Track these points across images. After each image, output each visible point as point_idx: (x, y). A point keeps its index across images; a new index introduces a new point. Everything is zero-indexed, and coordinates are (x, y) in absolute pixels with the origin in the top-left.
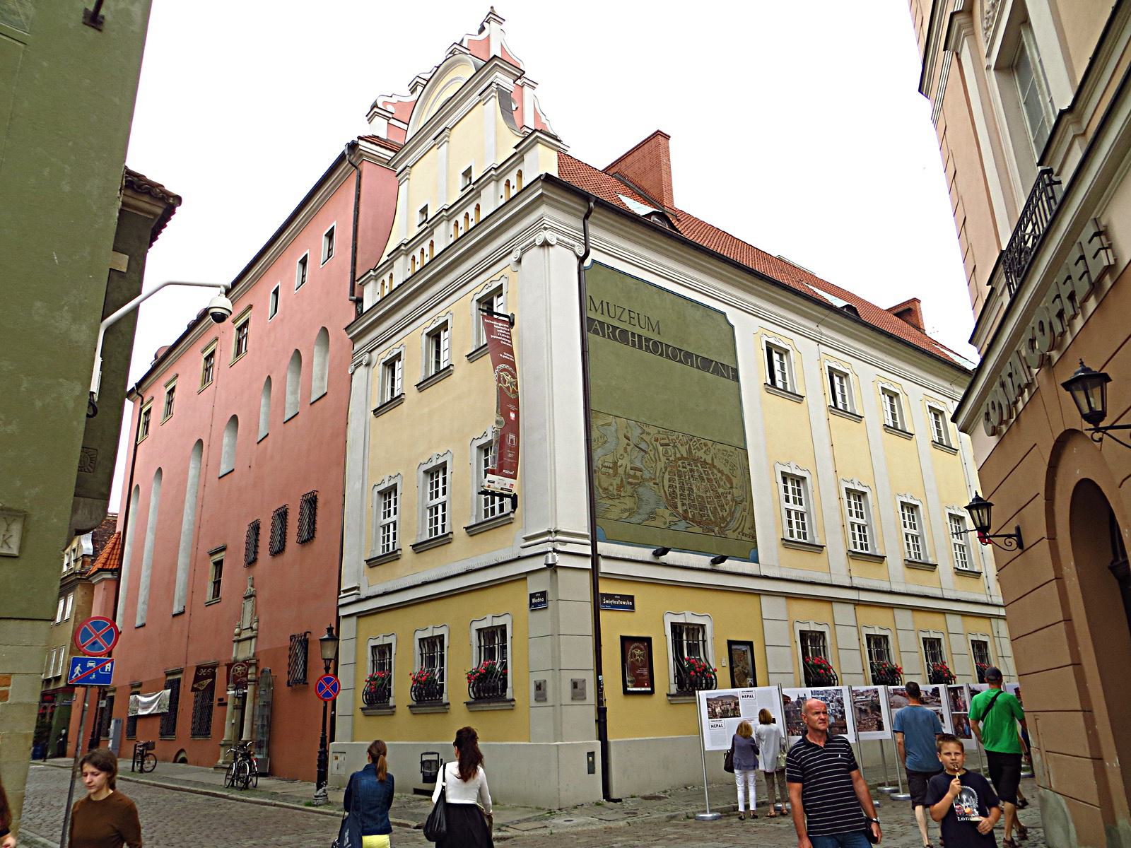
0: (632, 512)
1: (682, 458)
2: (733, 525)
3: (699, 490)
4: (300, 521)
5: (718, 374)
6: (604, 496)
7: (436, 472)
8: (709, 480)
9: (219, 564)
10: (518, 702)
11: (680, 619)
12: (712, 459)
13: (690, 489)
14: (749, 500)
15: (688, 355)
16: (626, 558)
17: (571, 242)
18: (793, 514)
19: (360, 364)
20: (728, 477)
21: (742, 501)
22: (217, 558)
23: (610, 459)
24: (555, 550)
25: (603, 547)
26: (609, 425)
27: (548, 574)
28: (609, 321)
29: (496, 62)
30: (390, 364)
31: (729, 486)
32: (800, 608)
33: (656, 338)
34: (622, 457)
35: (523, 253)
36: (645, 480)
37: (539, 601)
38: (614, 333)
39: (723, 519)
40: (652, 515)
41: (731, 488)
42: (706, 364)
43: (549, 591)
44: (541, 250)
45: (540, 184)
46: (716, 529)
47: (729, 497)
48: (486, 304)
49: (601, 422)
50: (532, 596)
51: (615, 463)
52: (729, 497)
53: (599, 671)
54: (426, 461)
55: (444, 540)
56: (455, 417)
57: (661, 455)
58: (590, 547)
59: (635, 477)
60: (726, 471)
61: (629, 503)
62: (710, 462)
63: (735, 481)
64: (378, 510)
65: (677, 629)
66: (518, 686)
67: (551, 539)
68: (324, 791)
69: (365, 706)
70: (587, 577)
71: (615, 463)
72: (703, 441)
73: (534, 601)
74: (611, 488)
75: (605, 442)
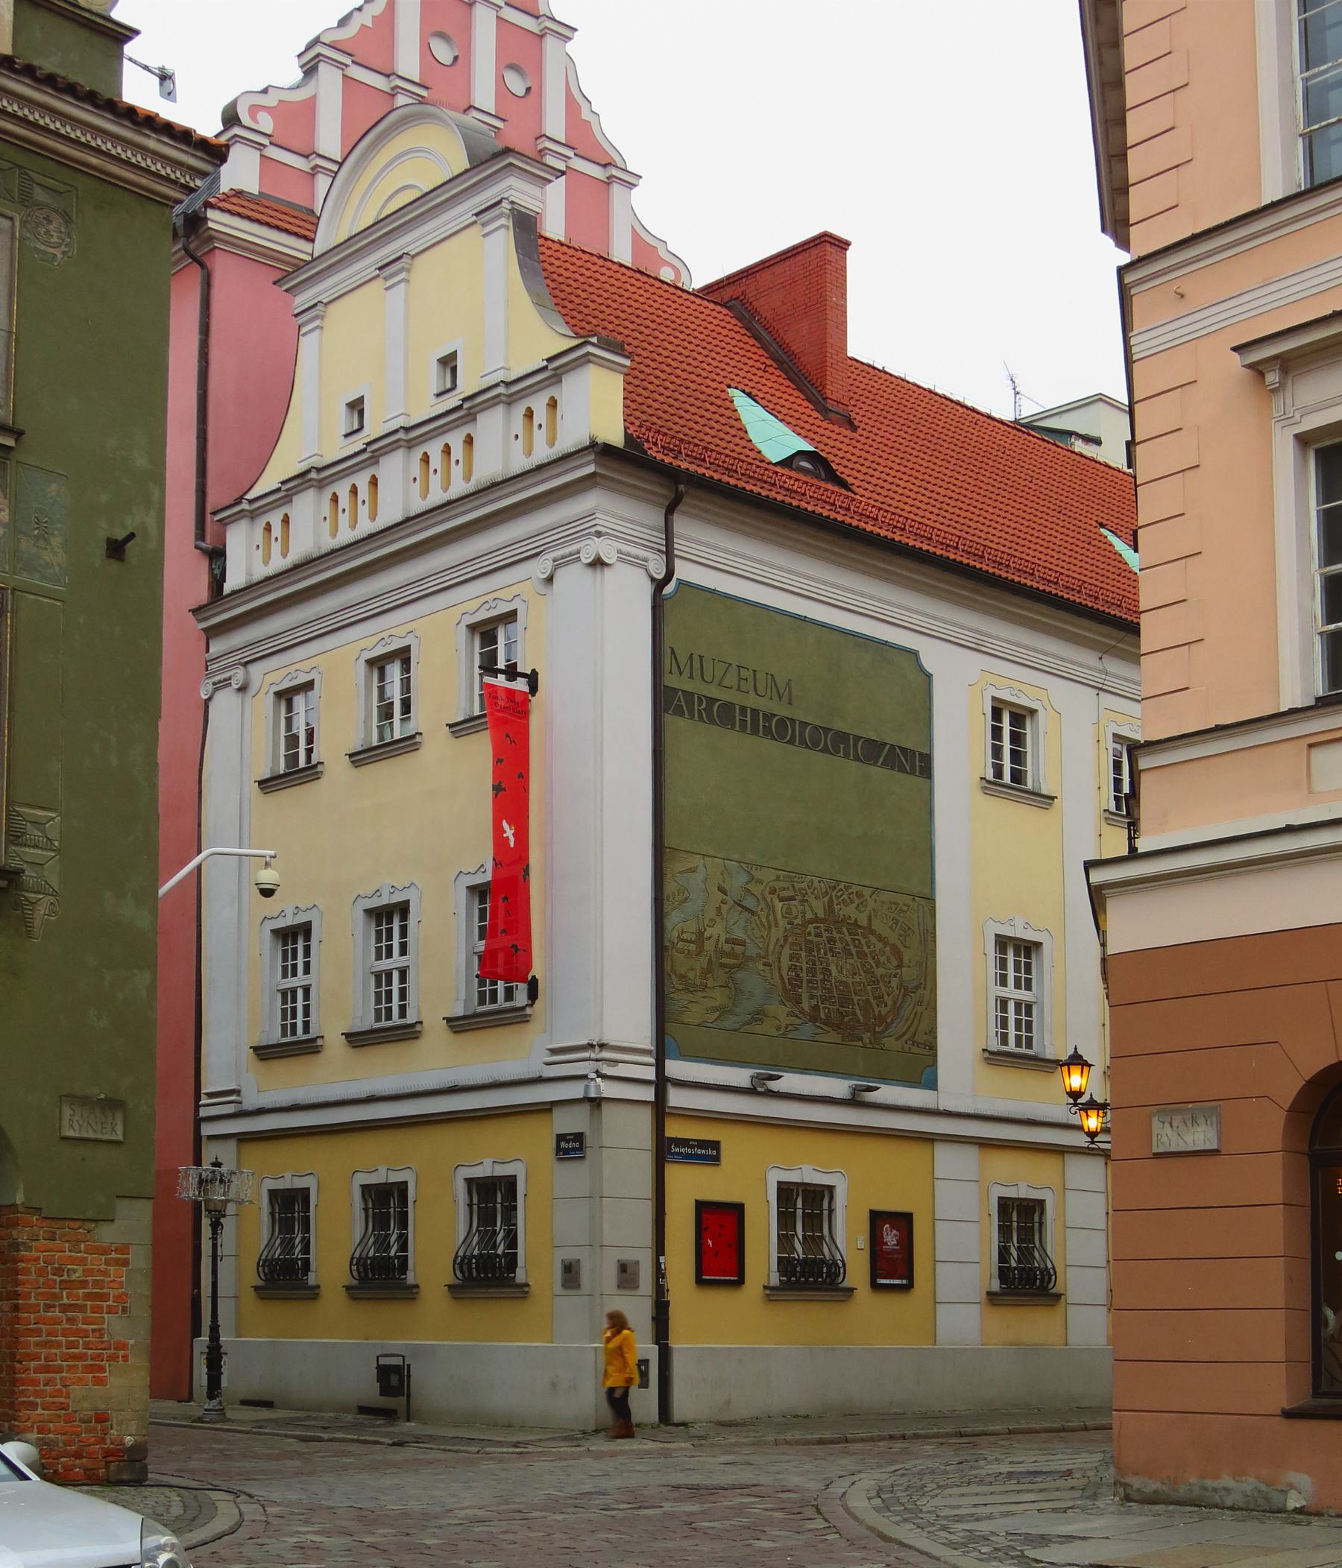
0: (723, 1011)
1: (816, 919)
3: (840, 972)
5: (893, 769)
6: (680, 987)
7: (389, 917)
8: (861, 955)
10: (535, 1288)
11: (793, 1177)
12: (870, 919)
13: (826, 971)
15: (841, 737)
16: (708, 1083)
17: (642, 553)
18: (1011, 1006)
19: (225, 683)
20: (894, 947)
21: (917, 988)
23: (692, 927)
24: (600, 1075)
25: (675, 1068)
26: (693, 870)
27: (586, 1108)
28: (698, 684)
29: (511, 160)
31: (896, 963)
32: (1003, 1164)
33: (781, 710)
34: (713, 923)
35: (556, 568)
36: (752, 959)
38: (709, 710)
39: (881, 1019)
40: (758, 1016)
41: (900, 966)
42: (874, 751)
43: (587, 1133)
44: (589, 572)
45: (592, 457)
46: (867, 1036)
47: (895, 982)
48: (486, 632)
50: (560, 1138)
51: (700, 934)
52: (895, 982)
53: (659, 1248)
54: (370, 893)
56: (426, 827)
57: (779, 916)
58: (653, 1069)
59: (731, 954)
61: (719, 997)
62: (865, 924)
64: (272, 967)
65: (786, 1191)
66: (536, 1264)
67: (593, 1056)
68: (220, 1403)
69: (260, 1283)
70: (646, 1116)
71: (700, 934)
72: (855, 889)
73: (563, 1145)
74: (691, 975)
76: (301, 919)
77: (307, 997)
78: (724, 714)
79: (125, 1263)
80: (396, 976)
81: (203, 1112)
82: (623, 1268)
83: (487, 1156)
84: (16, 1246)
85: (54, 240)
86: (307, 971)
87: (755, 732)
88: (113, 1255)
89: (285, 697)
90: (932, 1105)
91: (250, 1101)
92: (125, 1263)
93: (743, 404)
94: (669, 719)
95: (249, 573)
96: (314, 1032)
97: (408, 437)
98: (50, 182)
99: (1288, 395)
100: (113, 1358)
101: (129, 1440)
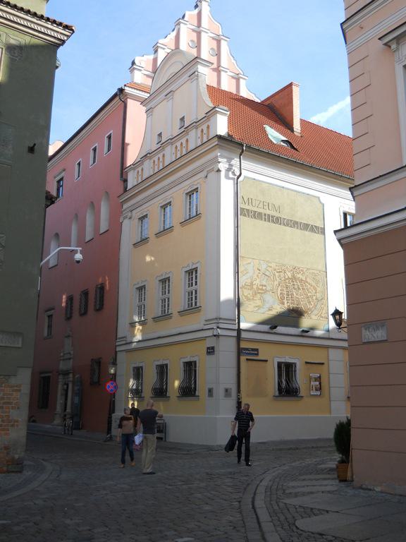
0: (259, 307)
2: (315, 312)
4: (96, 298)
7: (165, 281)
9: (50, 317)
11: (283, 360)
14: (326, 298)
15: (297, 223)
22: (49, 313)
23: (249, 281)
24: (218, 327)
26: (250, 263)
30: (142, 219)
31: (314, 291)
33: (276, 214)
37: (211, 351)
42: (306, 227)
47: (314, 297)
49: (245, 263)
50: (208, 348)
52: (314, 297)
59: (262, 289)
60: (313, 284)
61: (259, 303)
63: (318, 289)
66: (201, 390)
70: (234, 340)
75: (247, 273)
78: (258, 216)
79: (20, 391)
80: (167, 300)
81: (117, 344)
82: (226, 390)
85: (16, 55)
88: (16, 388)
92: (20, 391)
93: (268, 128)
97: (171, 141)
98: (15, 37)
99: (400, 52)
100: (13, 426)
101: (17, 456)
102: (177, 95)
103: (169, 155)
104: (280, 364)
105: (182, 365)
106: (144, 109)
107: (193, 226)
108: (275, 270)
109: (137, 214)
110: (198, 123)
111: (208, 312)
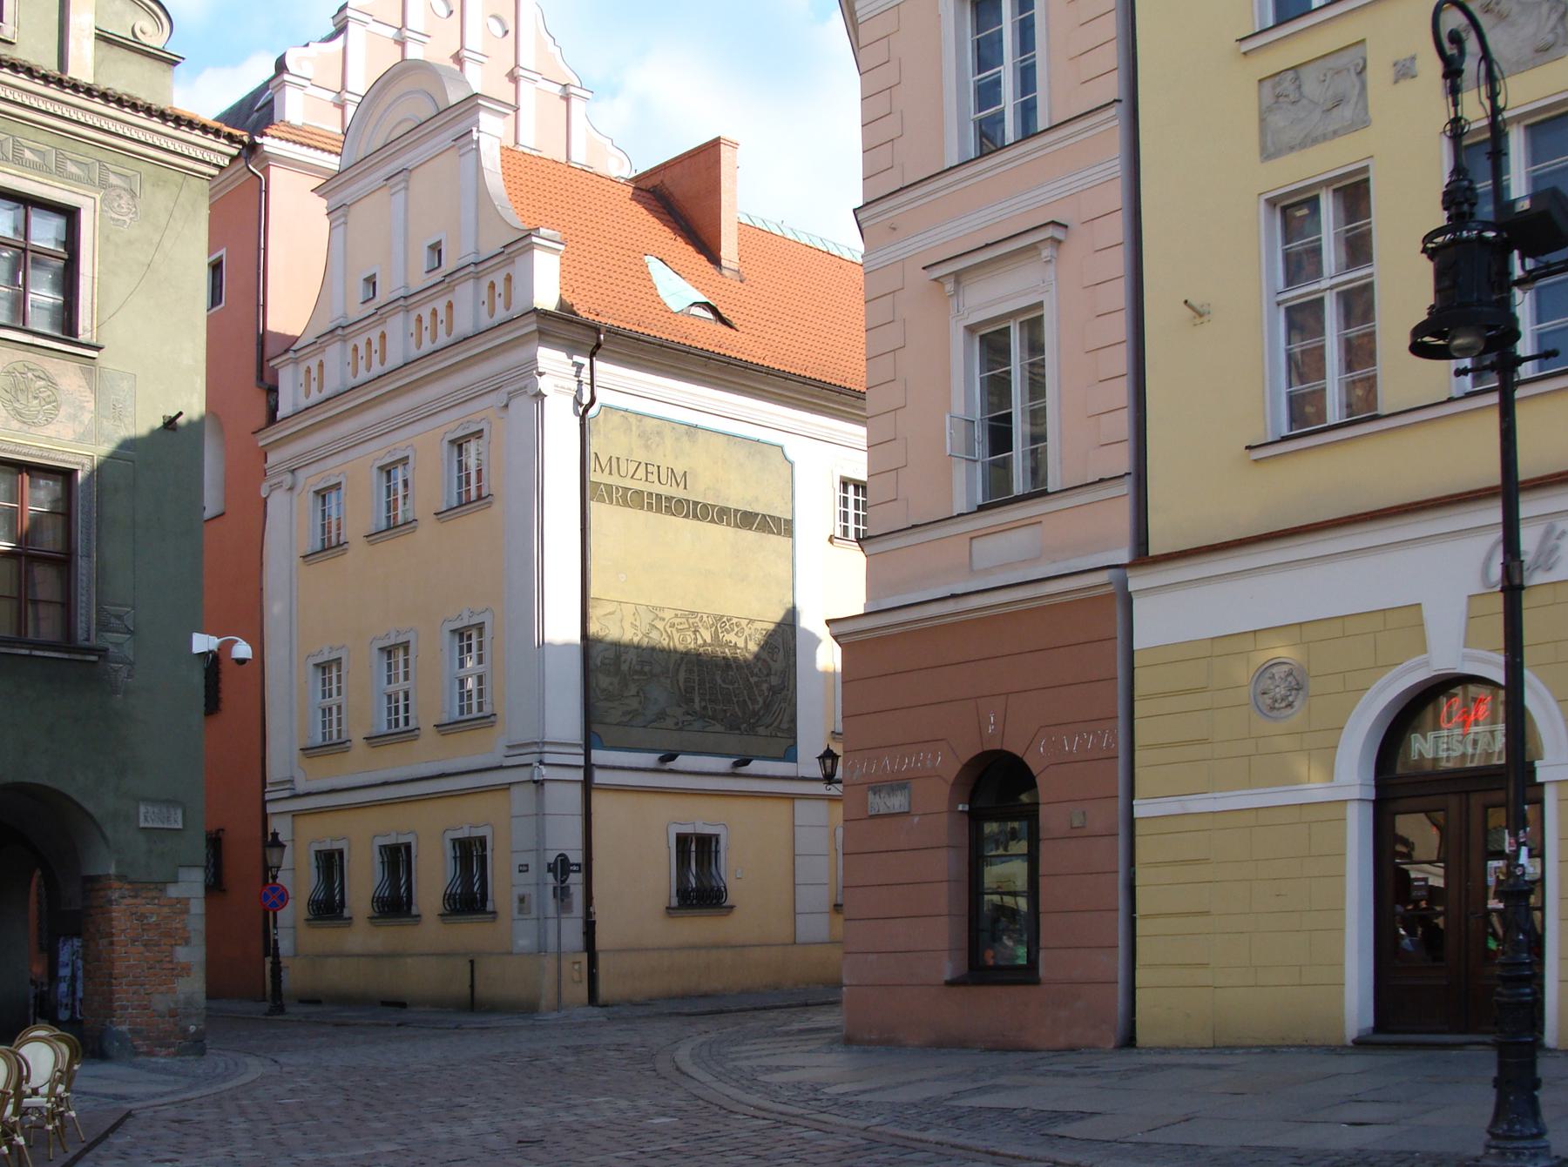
24: (541, 763)
25: (598, 756)
33: (679, 493)
39: (755, 713)
42: (747, 520)
47: (765, 686)
55: (411, 734)
76: (335, 656)
77: (339, 712)
82: (522, 900)
83: (469, 819)
84: (110, 902)
86: (339, 693)
87: (659, 510)
89: (322, 494)
90: (792, 773)
91: (301, 787)
93: (656, 268)
94: (593, 506)
95: (295, 405)
96: (344, 737)
97: (405, 301)
102: (419, 181)
103: (399, 341)
104: (682, 840)
105: (449, 845)
106: (324, 202)
107: (472, 522)
108: (672, 626)
109: (311, 479)
110: (481, 268)
111: (514, 727)
